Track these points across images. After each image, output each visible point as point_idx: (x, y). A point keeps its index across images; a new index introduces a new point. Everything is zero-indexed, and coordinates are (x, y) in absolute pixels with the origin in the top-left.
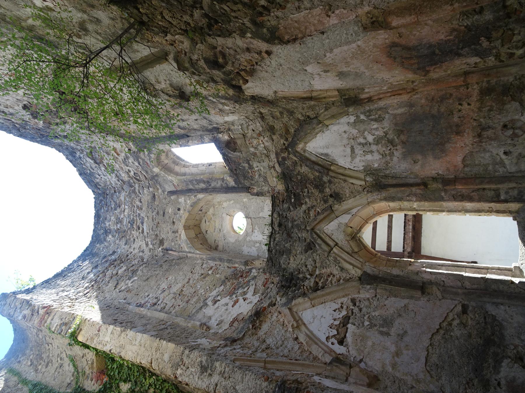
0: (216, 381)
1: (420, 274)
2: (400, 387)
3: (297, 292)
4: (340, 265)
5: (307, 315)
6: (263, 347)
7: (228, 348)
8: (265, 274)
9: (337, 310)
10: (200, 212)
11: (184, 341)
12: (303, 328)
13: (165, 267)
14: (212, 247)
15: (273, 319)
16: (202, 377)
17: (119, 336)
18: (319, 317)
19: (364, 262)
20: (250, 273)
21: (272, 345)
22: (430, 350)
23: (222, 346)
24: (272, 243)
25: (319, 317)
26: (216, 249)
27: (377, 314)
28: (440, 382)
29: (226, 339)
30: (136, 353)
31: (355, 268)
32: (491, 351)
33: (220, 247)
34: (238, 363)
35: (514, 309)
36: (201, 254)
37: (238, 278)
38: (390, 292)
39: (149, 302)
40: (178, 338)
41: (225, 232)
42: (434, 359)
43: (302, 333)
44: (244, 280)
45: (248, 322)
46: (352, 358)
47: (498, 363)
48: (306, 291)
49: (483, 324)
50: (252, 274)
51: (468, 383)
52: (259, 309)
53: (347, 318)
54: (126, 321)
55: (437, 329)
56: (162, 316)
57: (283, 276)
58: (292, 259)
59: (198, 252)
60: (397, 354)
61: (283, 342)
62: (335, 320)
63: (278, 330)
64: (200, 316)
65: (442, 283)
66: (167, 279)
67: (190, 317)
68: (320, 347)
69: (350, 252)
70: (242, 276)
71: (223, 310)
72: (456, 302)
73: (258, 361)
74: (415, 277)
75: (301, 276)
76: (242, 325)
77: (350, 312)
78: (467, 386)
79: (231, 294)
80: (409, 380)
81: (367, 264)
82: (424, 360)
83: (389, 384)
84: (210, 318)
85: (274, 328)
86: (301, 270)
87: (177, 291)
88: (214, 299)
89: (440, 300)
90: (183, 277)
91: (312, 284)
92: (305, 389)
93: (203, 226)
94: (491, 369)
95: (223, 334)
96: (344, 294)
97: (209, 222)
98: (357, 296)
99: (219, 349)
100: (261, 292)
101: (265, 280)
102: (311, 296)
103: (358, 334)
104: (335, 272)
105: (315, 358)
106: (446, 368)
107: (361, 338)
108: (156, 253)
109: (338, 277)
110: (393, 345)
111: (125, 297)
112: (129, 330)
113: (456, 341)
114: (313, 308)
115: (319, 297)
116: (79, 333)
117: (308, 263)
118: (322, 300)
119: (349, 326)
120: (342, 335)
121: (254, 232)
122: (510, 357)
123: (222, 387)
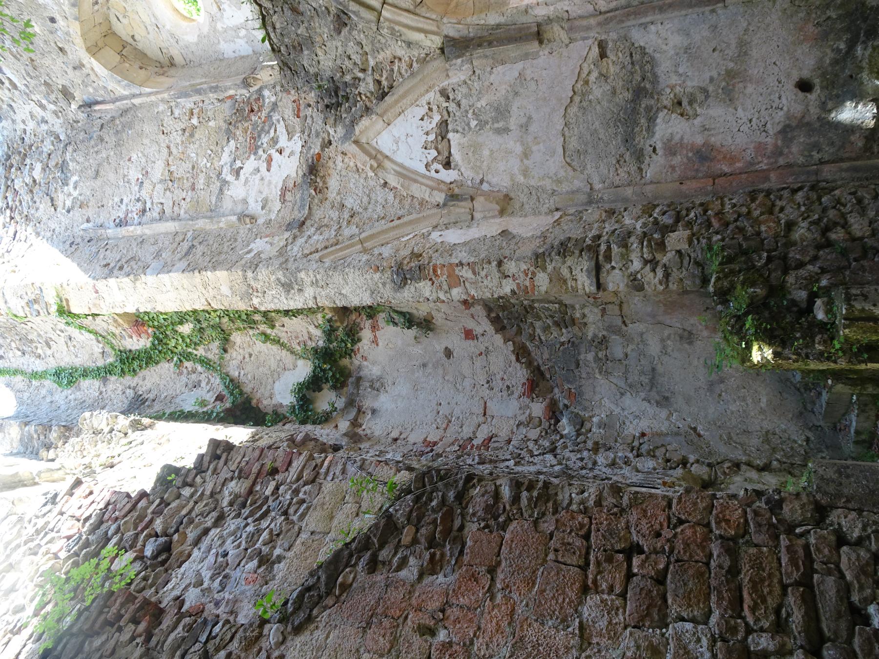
0: (312, 294)
1: (530, 11)
2: (538, 198)
3: (353, 109)
4: (403, 38)
5: (385, 142)
6: (346, 216)
7: (300, 241)
8: (289, 93)
9: (426, 117)
10: (96, 7)
11: (234, 258)
12: (387, 164)
13: (111, 139)
14: (165, 65)
15: (339, 168)
16: (291, 296)
17: (135, 288)
18: (403, 138)
19: (439, 19)
20: (264, 100)
21: (357, 208)
22: (567, 133)
23: (290, 241)
24: (272, 35)
25: (402, 136)
26: (172, 64)
27: (483, 102)
28: (586, 172)
29: (289, 227)
30: (178, 300)
31: (429, 35)
32: (643, 106)
33: (178, 59)
34: (328, 262)
35: (669, 26)
36: (157, 93)
37: (248, 116)
38: (493, 58)
39: (132, 211)
40: (223, 256)
41: (168, 27)
42: (573, 144)
43: (390, 173)
44: (259, 118)
45: (305, 187)
46: (469, 182)
47: (652, 120)
48: (368, 104)
49: (630, 66)
50: (267, 101)
51: (618, 162)
52: (310, 160)
53: (444, 124)
54: (124, 260)
55: (571, 98)
56: (170, 226)
57: (320, 87)
58: (320, 53)
59: (148, 90)
60: (526, 155)
61: (368, 196)
62: (427, 134)
63: (353, 180)
64: (227, 205)
65: (565, 15)
66: (129, 160)
67: (213, 213)
68: (422, 184)
69: (412, 7)
70: (252, 111)
71: (257, 181)
72: (590, 42)
73: (352, 245)
74: (524, 19)
75: (348, 78)
76: (299, 196)
77: (445, 113)
78: (617, 166)
79: (254, 149)
80: (548, 184)
81: (445, 20)
82: (561, 150)
83: (525, 200)
84: (245, 201)
85: (345, 176)
86: (344, 67)
87: (162, 175)
88: (232, 170)
89: (567, 46)
90: (155, 147)
91: (371, 87)
92: (429, 263)
93: (122, 29)
94: (644, 133)
95: (279, 220)
96: (426, 87)
97: (125, 17)
98: (446, 83)
99: (289, 248)
100: (298, 129)
101: (295, 105)
102: (379, 110)
103: (466, 144)
104: (400, 53)
105: (422, 203)
106: (590, 151)
107: (472, 149)
108: (71, 116)
109: (407, 59)
110: (518, 144)
111: (85, 218)
112: (142, 276)
113: (598, 107)
114: (390, 127)
115: (391, 107)
116: (68, 305)
117: (350, 52)
118: (398, 109)
119: (450, 135)
120: (446, 154)
121: (224, 10)
122: (665, 107)
123: (324, 298)
